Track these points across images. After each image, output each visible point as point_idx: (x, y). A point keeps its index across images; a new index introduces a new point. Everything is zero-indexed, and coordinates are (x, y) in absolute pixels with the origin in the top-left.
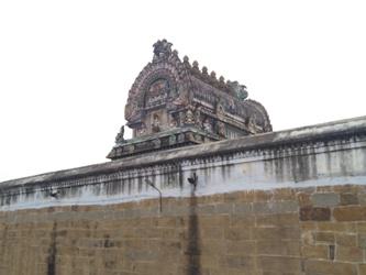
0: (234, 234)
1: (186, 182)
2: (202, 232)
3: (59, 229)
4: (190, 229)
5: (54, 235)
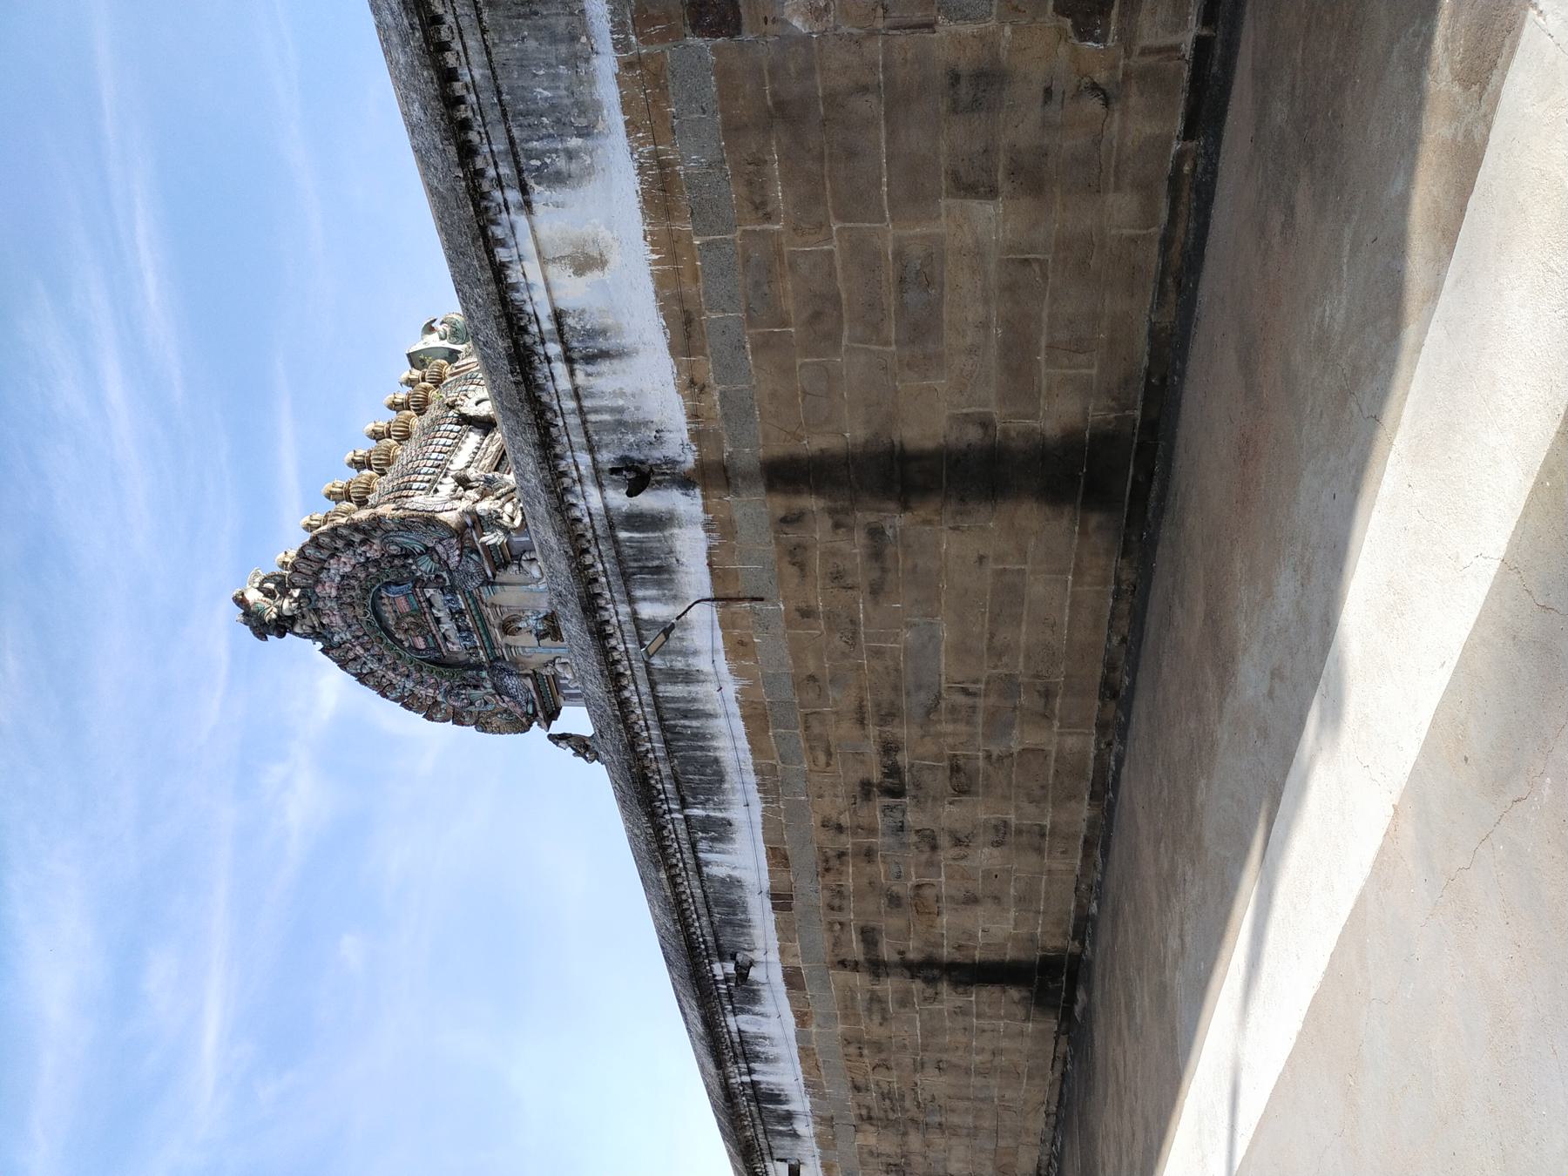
0: (817, 316)
1: (648, 501)
2: (815, 443)
3: (856, 950)
4: (817, 490)
5: (876, 967)
